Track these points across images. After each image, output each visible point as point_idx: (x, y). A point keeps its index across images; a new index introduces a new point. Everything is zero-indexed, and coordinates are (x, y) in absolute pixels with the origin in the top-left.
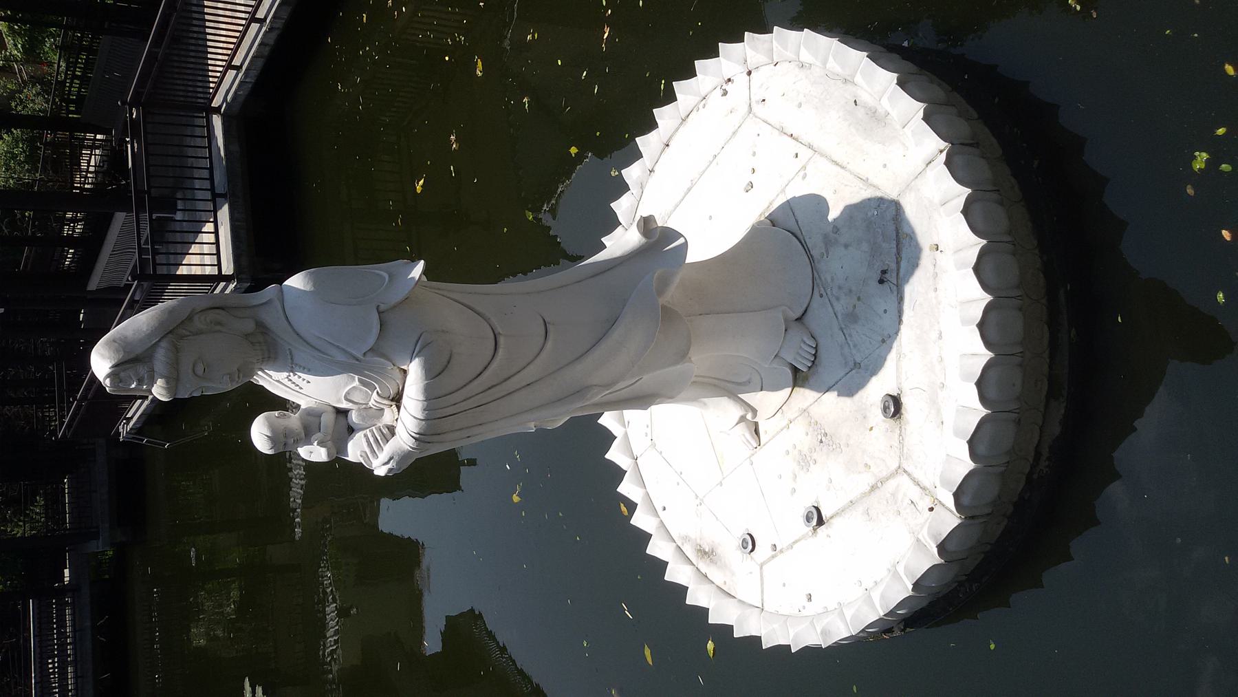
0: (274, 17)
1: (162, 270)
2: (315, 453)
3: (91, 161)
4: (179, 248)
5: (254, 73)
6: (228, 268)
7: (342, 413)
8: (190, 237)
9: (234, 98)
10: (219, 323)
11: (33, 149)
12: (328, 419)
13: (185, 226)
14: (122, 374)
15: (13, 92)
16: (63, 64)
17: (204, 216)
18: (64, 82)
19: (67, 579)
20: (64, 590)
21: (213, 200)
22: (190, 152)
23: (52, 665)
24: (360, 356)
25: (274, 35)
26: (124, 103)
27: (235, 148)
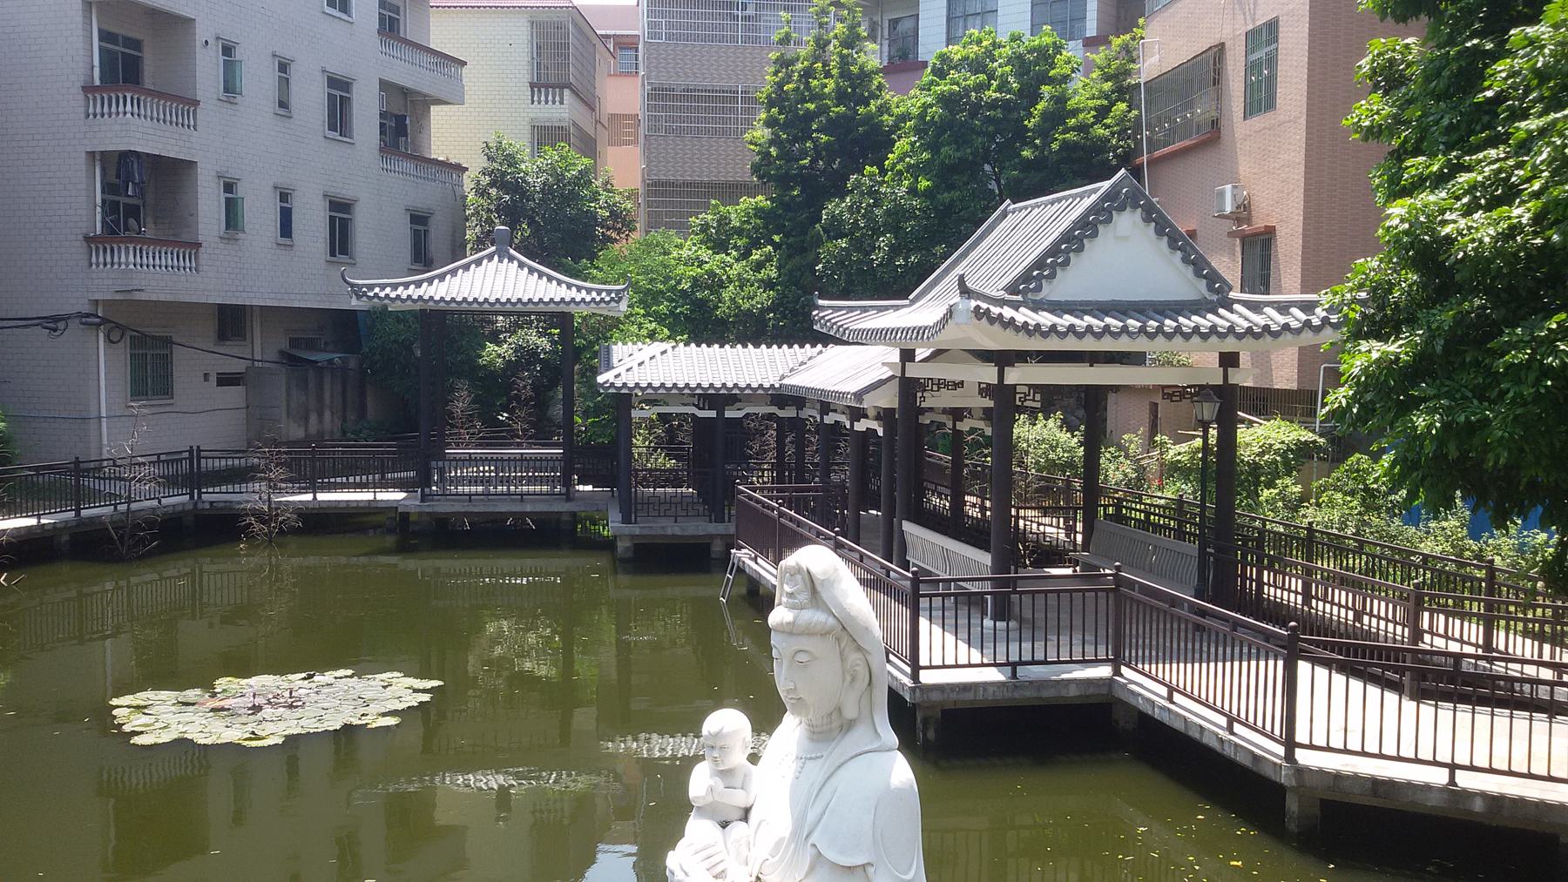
0: (1236, 745)
1: (924, 603)
2: (700, 783)
3: (1052, 530)
4: (950, 621)
5: (1166, 719)
6: (926, 677)
7: (745, 815)
8: (963, 634)
9: (1133, 692)
10: (853, 680)
11: (1063, 467)
12: (739, 799)
13: (976, 630)
14: (799, 577)
15: (1126, 450)
16: (1162, 502)
17: (989, 651)
18: (1141, 503)
19: (581, 488)
20: (568, 483)
21: (1007, 664)
22: (1065, 639)
23: (487, 470)
24: (812, 840)
25: (1214, 744)
26: (1118, 568)
27: (1073, 692)
